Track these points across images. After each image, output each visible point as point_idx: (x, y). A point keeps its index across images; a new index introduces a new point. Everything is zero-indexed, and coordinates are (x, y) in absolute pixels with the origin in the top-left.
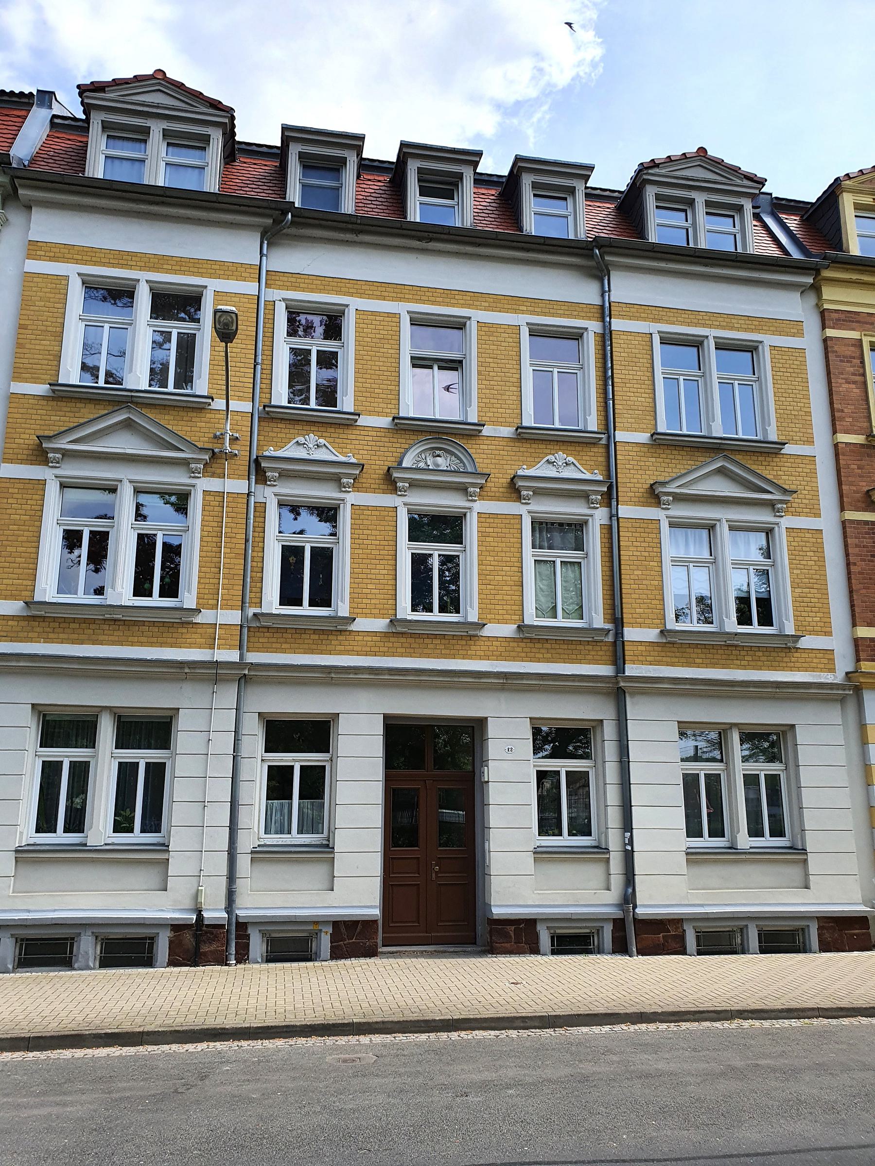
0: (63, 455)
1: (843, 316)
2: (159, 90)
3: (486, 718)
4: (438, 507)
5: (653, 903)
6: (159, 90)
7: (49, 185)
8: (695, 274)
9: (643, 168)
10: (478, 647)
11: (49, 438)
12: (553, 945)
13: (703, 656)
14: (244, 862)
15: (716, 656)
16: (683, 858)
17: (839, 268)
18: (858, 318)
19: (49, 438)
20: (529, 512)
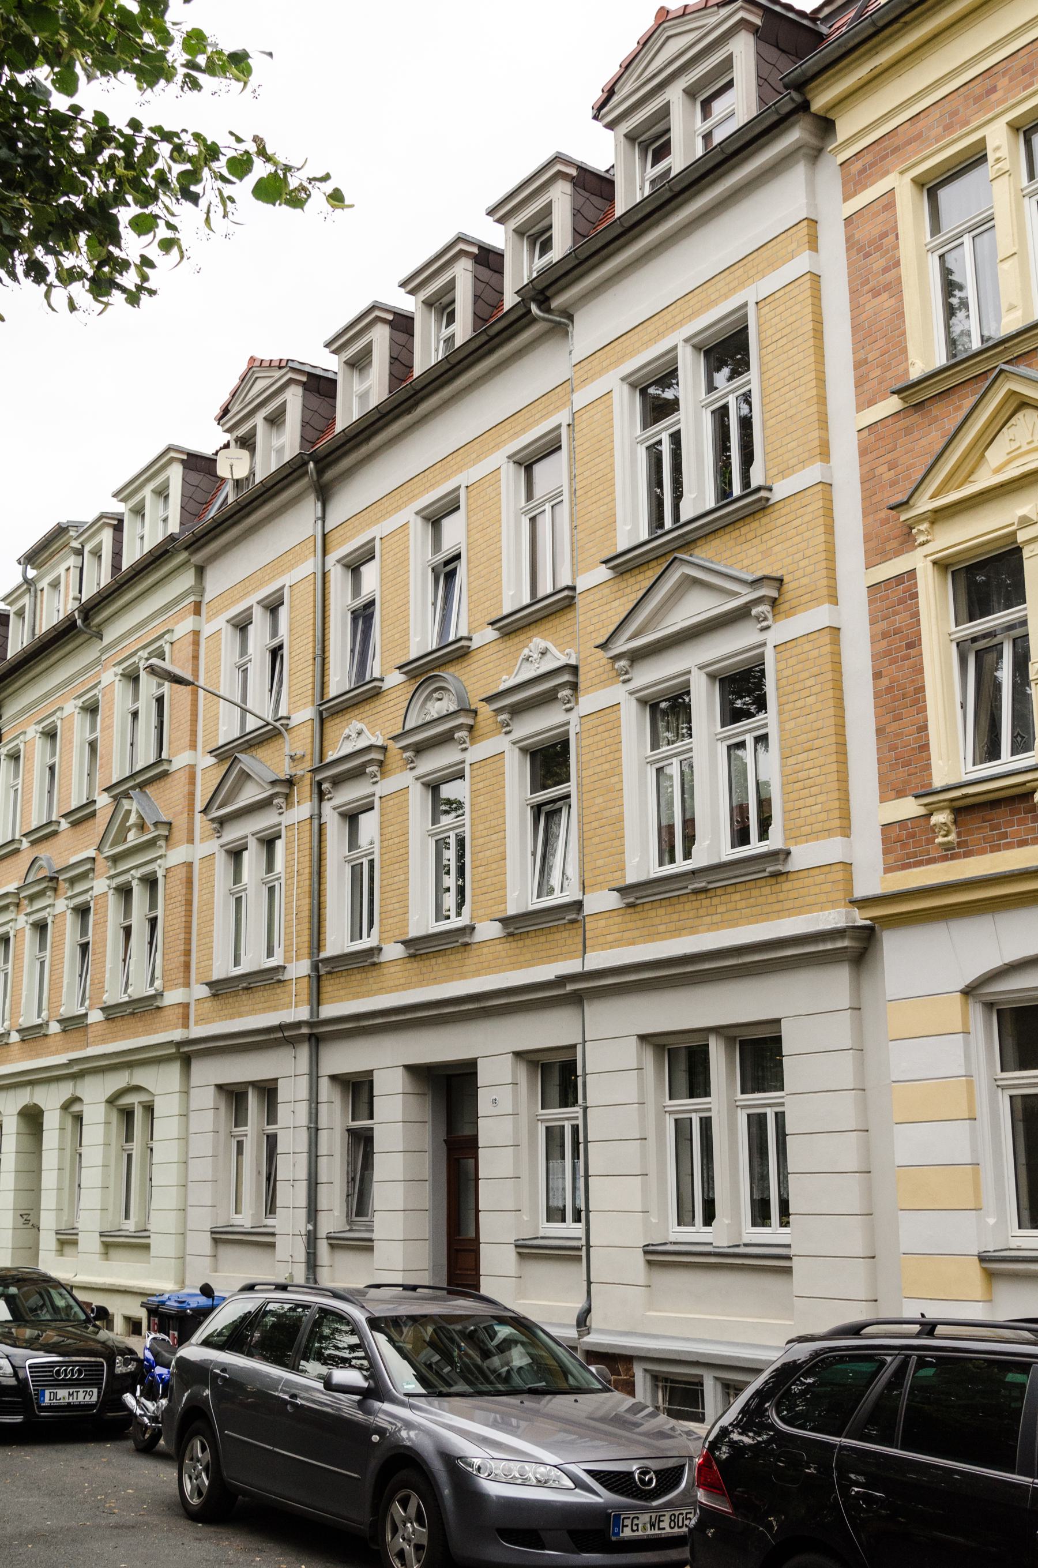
0: (933, 523)
1: (868, 158)
2: (669, 38)
3: (370, 1072)
4: (450, 767)
5: (607, 1328)
6: (669, 38)
7: (285, 482)
8: (671, 236)
9: (60, 531)
10: (472, 959)
11: (904, 505)
12: (702, 1391)
13: (666, 919)
14: (323, 1246)
15: (684, 915)
16: (640, 1258)
17: (848, 65)
18: (897, 141)
19: (904, 505)
20: (334, 809)
